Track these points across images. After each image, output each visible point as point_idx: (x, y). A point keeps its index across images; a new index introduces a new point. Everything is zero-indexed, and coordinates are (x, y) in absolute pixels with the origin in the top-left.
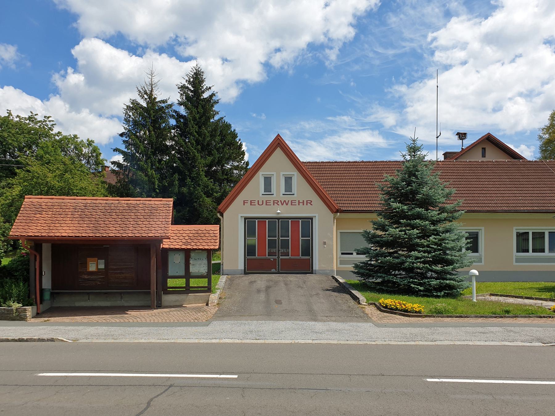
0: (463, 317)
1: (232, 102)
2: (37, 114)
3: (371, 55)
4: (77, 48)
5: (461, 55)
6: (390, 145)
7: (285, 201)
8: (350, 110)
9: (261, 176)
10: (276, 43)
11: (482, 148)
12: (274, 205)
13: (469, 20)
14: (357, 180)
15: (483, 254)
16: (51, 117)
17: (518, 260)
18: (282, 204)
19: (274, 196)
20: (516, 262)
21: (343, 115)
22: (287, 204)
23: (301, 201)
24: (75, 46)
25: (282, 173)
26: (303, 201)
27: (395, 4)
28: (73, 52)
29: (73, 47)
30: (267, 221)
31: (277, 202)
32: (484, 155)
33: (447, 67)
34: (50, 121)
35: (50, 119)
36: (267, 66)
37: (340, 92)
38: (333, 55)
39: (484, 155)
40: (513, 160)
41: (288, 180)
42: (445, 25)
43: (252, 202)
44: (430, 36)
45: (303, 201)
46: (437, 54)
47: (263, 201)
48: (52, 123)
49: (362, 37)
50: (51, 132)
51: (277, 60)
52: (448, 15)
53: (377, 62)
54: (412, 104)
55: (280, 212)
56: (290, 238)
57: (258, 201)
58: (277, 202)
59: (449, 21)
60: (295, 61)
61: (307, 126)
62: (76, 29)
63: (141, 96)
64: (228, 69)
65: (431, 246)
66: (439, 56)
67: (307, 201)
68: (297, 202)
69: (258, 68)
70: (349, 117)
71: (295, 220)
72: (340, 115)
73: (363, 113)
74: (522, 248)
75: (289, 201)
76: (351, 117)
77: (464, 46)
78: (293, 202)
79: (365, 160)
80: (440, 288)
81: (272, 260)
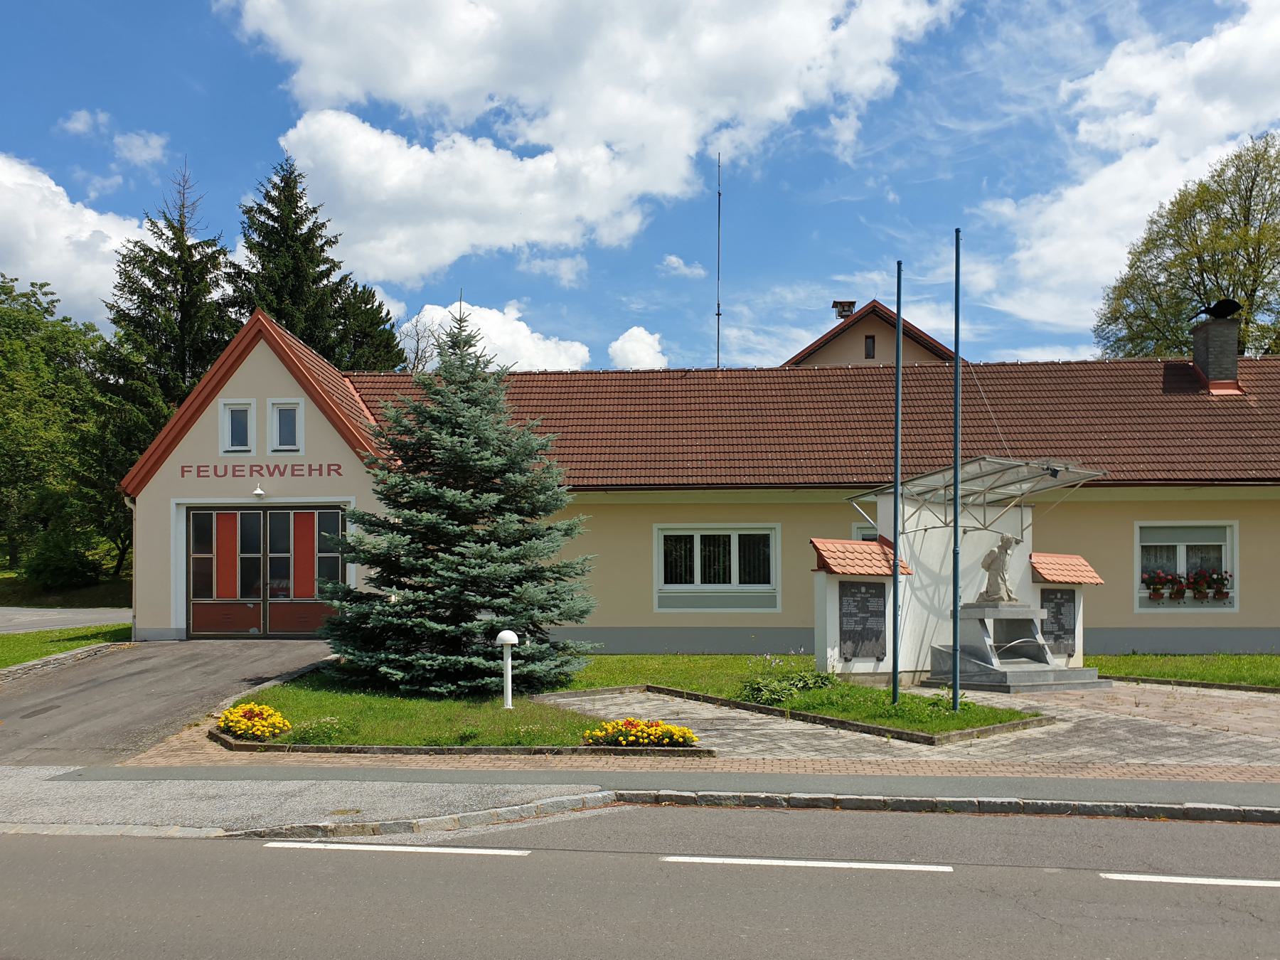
0: (353, 752)
1: (626, 245)
2: (17, 279)
3: (931, 135)
4: (292, 134)
5: (1142, 126)
6: (980, 335)
7: (277, 467)
8: (885, 257)
9: (221, 406)
10: (722, 113)
11: (867, 337)
12: (251, 475)
13: (1160, 46)
14: (872, 412)
15: (779, 589)
16: (48, 284)
17: (664, 601)
18: (271, 474)
19: (253, 454)
20: (775, 607)
21: (869, 270)
22: (282, 474)
23: (315, 466)
24: (288, 130)
25: (270, 401)
26: (321, 466)
27: (983, 20)
28: (282, 142)
29: (284, 131)
30: (316, 513)
31: (259, 468)
32: (870, 354)
33: (1109, 157)
34: (46, 294)
35: (46, 289)
36: (702, 163)
37: (862, 219)
38: (846, 131)
39: (870, 354)
40: (939, 363)
41: (287, 419)
42: (1101, 63)
43: (202, 469)
44: (1066, 88)
45: (321, 466)
46: (1083, 126)
47: (226, 467)
48: (50, 298)
49: (909, 95)
50: (50, 319)
51: (724, 147)
52: (1105, 39)
53: (944, 151)
54: (1027, 243)
55: (262, 492)
56: (291, 555)
57: (215, 467)
58: (336, 467)
59: (1110, 53)
60: (766, 151)
61: (789, 296)
62: (286, 93)
63: (155, 233)
64: (621, 169)
65: (439, 572)
66: (1087, 131)
67: (329, 466)
68: (306, 469)
69: (683, 168)
70: (885, 273)
71: (303, 511)
72: (862, 269)
73: (916, 265)
74: (676, 571)
75: (286, 466)
76: (887, 275)
77: (1149, 106)
78: (296, 468)
79: (549, 370)
80: (444, 674)
81: (251, 606)
